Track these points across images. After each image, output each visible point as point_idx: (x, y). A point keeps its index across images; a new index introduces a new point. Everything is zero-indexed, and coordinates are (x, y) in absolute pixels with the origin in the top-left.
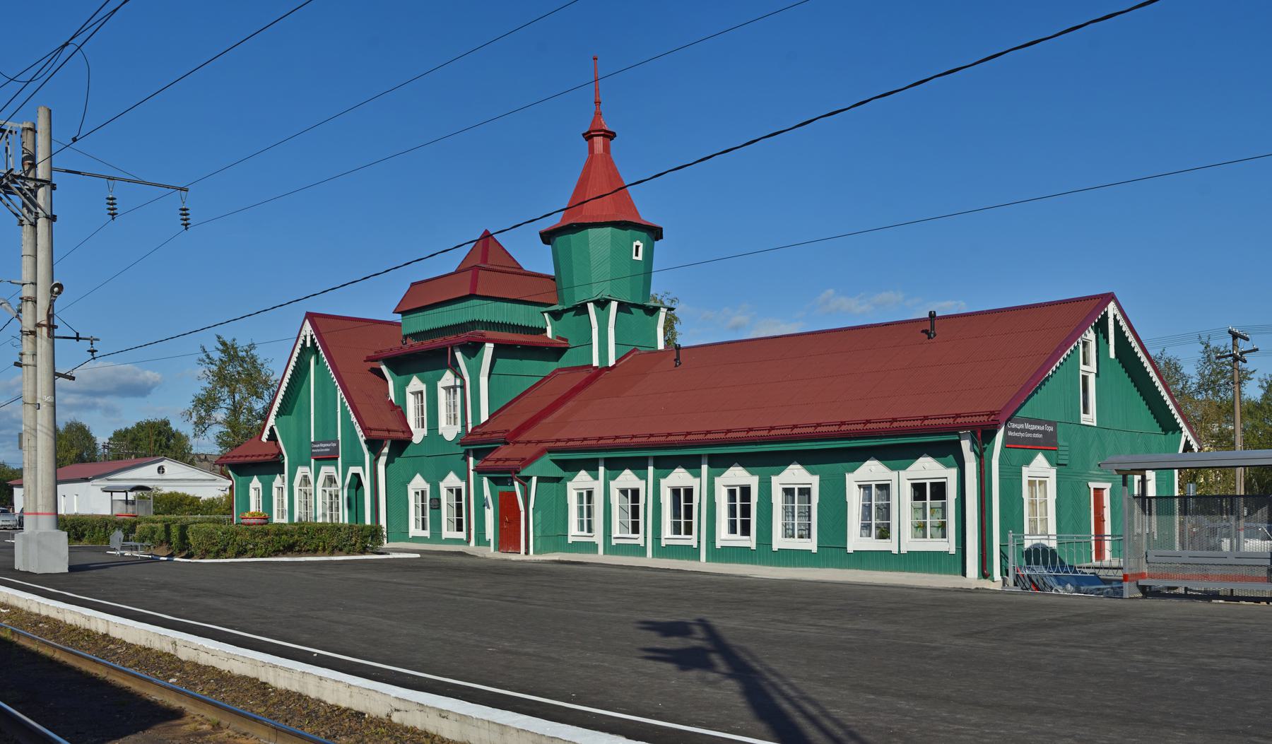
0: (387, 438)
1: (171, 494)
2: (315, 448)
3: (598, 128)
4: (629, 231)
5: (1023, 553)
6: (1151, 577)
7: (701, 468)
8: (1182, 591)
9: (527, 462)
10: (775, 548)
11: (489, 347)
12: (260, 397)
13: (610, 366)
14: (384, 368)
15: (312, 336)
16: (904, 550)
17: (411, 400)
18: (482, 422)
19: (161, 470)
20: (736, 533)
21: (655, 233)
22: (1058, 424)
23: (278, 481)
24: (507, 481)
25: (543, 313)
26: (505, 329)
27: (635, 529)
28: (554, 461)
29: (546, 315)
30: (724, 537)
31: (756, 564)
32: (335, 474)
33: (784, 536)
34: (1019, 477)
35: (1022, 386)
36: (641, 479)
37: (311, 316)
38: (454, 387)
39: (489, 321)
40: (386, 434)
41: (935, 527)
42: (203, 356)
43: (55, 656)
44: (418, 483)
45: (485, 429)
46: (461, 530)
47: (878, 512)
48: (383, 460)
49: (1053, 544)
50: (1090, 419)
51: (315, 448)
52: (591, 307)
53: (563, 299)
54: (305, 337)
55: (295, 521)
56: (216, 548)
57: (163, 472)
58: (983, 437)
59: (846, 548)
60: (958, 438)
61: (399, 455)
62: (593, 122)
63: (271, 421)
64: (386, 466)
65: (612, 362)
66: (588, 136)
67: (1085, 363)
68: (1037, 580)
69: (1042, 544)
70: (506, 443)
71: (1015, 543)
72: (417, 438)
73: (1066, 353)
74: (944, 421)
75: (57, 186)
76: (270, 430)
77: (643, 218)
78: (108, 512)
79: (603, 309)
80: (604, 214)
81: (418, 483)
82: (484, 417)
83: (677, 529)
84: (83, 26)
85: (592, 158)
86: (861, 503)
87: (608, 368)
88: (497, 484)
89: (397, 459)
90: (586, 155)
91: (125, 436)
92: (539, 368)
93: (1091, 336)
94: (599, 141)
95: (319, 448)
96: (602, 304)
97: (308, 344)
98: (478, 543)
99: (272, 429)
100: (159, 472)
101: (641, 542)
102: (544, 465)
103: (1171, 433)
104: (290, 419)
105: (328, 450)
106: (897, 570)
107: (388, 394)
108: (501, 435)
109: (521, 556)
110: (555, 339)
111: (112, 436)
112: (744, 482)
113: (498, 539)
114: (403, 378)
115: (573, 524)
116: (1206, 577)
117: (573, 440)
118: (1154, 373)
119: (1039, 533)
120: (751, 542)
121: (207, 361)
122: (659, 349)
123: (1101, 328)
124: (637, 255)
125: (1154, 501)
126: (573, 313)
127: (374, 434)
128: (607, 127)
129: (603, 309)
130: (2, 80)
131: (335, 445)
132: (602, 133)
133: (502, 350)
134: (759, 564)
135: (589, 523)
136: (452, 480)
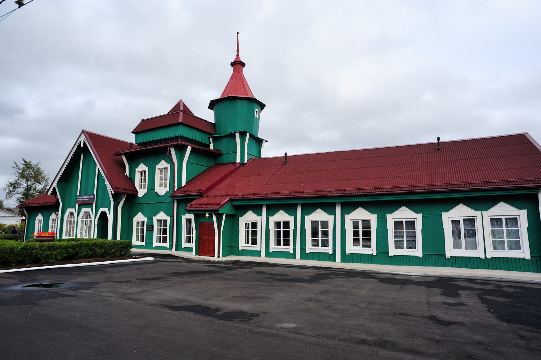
0: (124, 194)
11: (189, 148)
12: (40, 183)
18: (182, 186)
20: (191, 243)
23: (53, 216)
27: (254, 242)
30: (351, 248)
33: (188, 241)
34: (428, 145)
36: (258, 216)
40: (125, 191)
42: (15, 166)
52: (248, 135)
54: (80, 142)
59: (445, 255)
65: (246, 162)
67: (256, 115)
75: (30, 160)
76: (53, 189)
81: (133, 250)
82: (184, 183)
83: (278, 243)
84: (6, 17)
95: (82, 199)
97: (82, 145)
98: (177, 250)
99: (54, 189)
105: (88, 199)
109: (215, 258)
120: (373, 250)
124: (189, 222)
126: (377, 280)
127: (119, 191)
136: (162, 216)
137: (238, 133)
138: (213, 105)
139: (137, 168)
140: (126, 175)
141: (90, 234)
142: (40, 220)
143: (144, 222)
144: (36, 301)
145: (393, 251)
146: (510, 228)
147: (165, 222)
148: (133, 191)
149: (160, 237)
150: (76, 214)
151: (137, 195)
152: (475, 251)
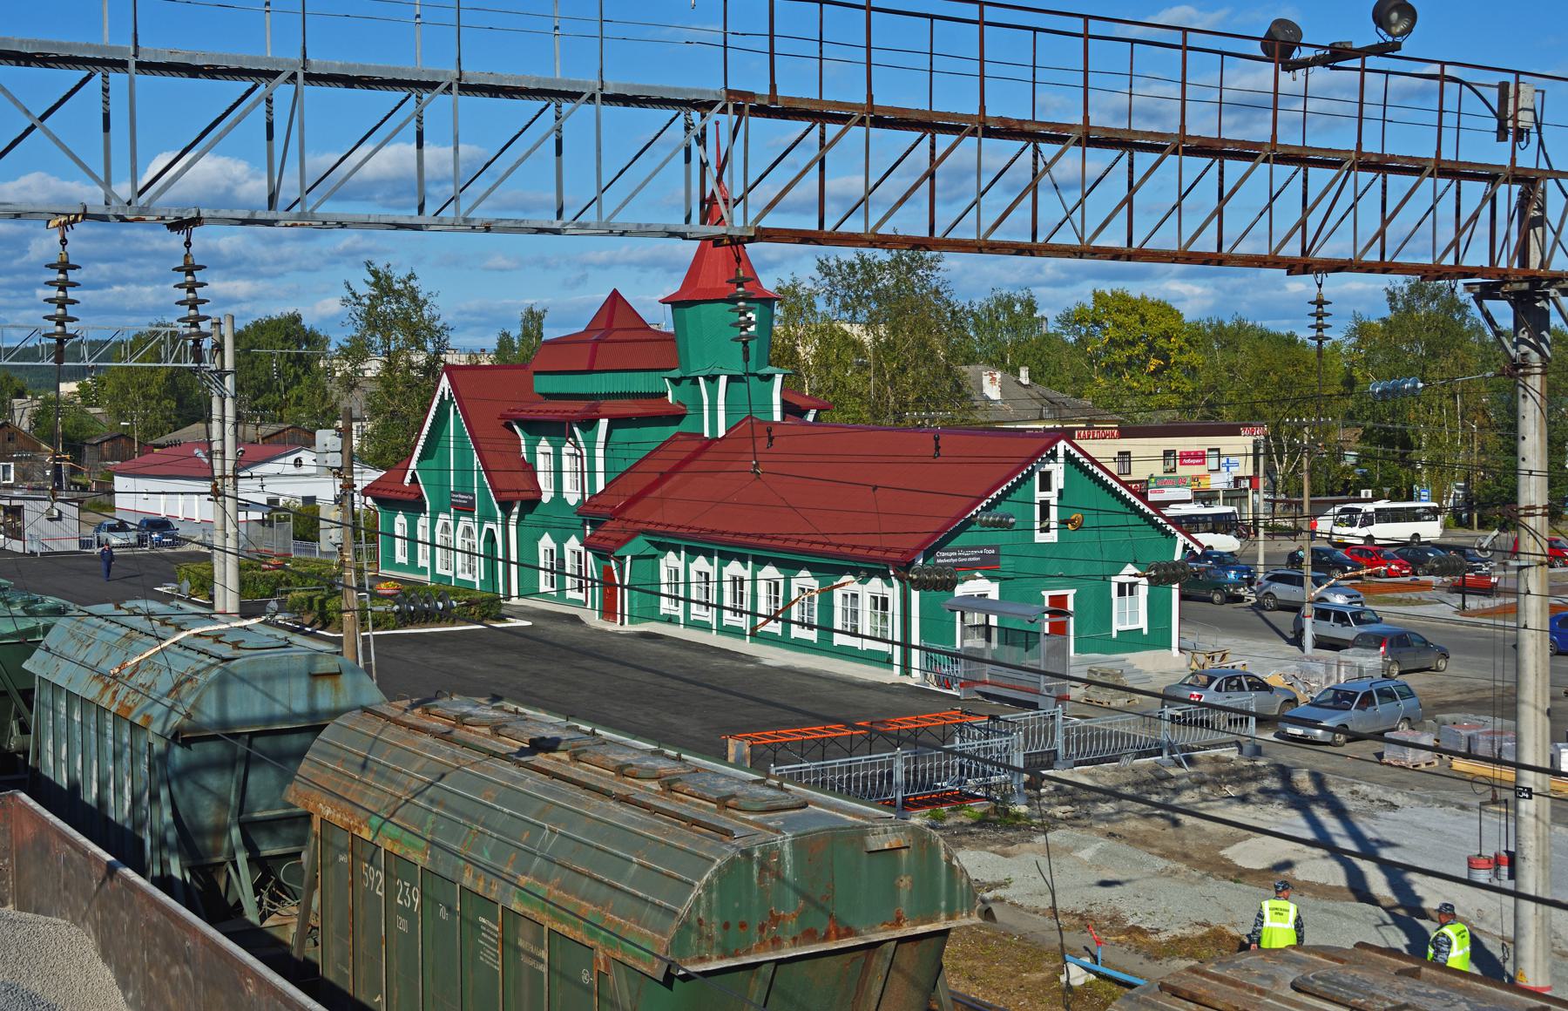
8: (1106, 705)
9: (621, 543)
11: (603, 424)
19: (298, 463)
24: (608, 559)
40: (515, 495)
43: (234, 713)
44: (546, 542)
48: (514, 518)
51: (1339, 670)
52: (701, 380)
55: (1177, 586)
65: (721, 433)
68: (176, 444)
72: (546, 498)
81: (546, 542)
82: (600, 486)
87: (717, 439)
89: (528, 517)
92: (655, 435)
96: (711, 379)
99: (413, 474)
101: (709, 619)
104: (431, 463)
119: (731, 759)
121: (354, 300)
127: (506, 496)
130: (1565, 183)
138: (676, 303)
143: (552, 551)
144: (755, 867)
150: (451, 524)
152: (1548, 651)
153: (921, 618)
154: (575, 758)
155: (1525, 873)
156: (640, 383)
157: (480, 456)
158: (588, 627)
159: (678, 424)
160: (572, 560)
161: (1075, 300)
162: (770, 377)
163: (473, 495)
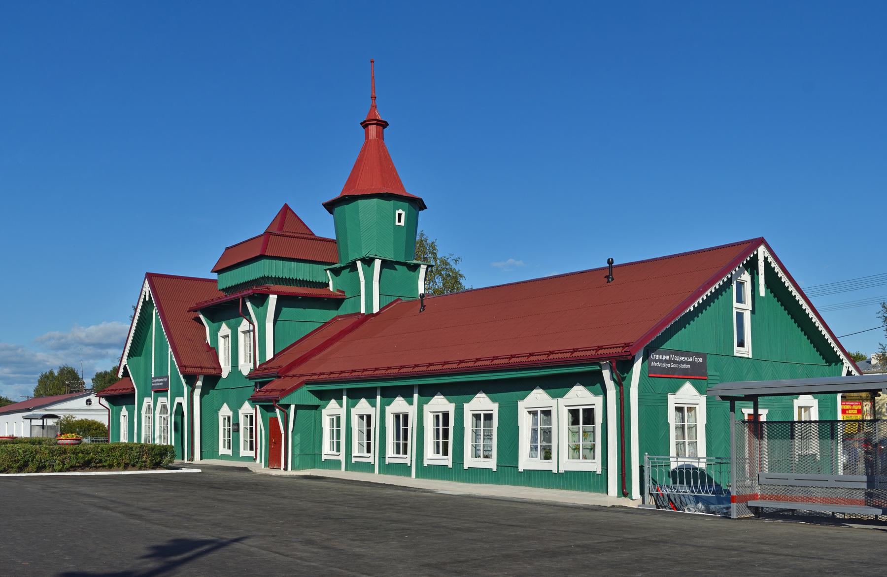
1: (82, 420)
2: (154, 383)
3: (373, 118)
4: (392, 202)
5: (669, 473)
6: (763, 498)
7: (376, 398)
9: (285, 392)
10: (466, 467)
11: (273, 299)
13: (374, 313)
14: (201, 316)
15: (149, 292)
16: (562, 470)
17: (221, 342)
18: (267, 360)
19: (89, 402)
21: (417, 204)
22: (708, 356)
25: (326, 270)
26: (290, 284)
28: (311, 391)
29: (328, 272)
30: (431, 456)
31: (452, 480)
32: (167, 403)
35: (660, 320)
37: (150, 276)
38: (249, 331)
39: (277, 277)
40: (199, 370)
41: (588, 449)
45: (269, 366)
46: (253, 450)
47: (544, 435)
48: (197, 392)
49: (702, 465)
50: (747, 351)
51: (154, 383)
52: (359, 263)
53: (341, 262)
56: (18, 464)
57: (90, 404)
58: (622, 368)
59: (518, 467)
60: (599, 368)
61: (213, 388)
62: (369, 114)
63: (124, 362)
64: (201, 396)
65: (376, 309)
66: (365, 125)
68: (675, 500)
69: (693, 466)
70: (279, 377)
71: (650, 465)
72: (224, 375)
73: (710, 290)
74: (588, 353)
77: (407, 191)
78: (41, 436)
79: (369, 266)
80: (373, 188)
82: (270, 355)
85: (367, 142)
86: (581, 408)
87: (373, 315)
88: (268, 411)
90: (363, 140)
91: (104, 377)
92: (320, 316)
93: (746, 277)
94: (373, 129)
96: (368, 262)
97: (147, 299)
99: (125, 368)
100: (87, 404)
101: (371, 460)
102: (304, 396)
103: (834, 364)
105: (161, 384)
106: (557, 488)
107: (205, 338)
108: (275, 370)
109: (281, 472)
110: (336, 292)
111: (95, 377)
112: (444, 409)
113: (268, 457)
114: (216, 324)
115: (429, 445)
116: (810, 499)
117: (324, 374)
118: (810, 310)
119: (687, 456)
122: (759, 410)
123: (752, 267)
124: (399, 221)
125: (765, 426)
126: (348, 270)
127: (189, 370)
128: (380, 118)
129: (369, 266)
131: (166, 380)
132: (376, 122)
133: (284, 301)
134: (455, 480)
135: (405, 445)
137: (380, 260)
139: (240, 409)
140: (208, 343)
141: (167, 443)
142: (335, 417)
143: (229, 418)
145: (469, 461)
146: (483, 453)
147: (446, 415)
148: (215, 369)
149: (333, 430)
151: (221, 376)
153: (279, 427)
154: (721, 381)
155: (598, 504)
156: (304, 272)
157: (172, 347)
158: (253, 473)
159: (337, 308)
160: (245, 423)
161: (210, 394)
162: (415, 268)
163: (167, 377)
